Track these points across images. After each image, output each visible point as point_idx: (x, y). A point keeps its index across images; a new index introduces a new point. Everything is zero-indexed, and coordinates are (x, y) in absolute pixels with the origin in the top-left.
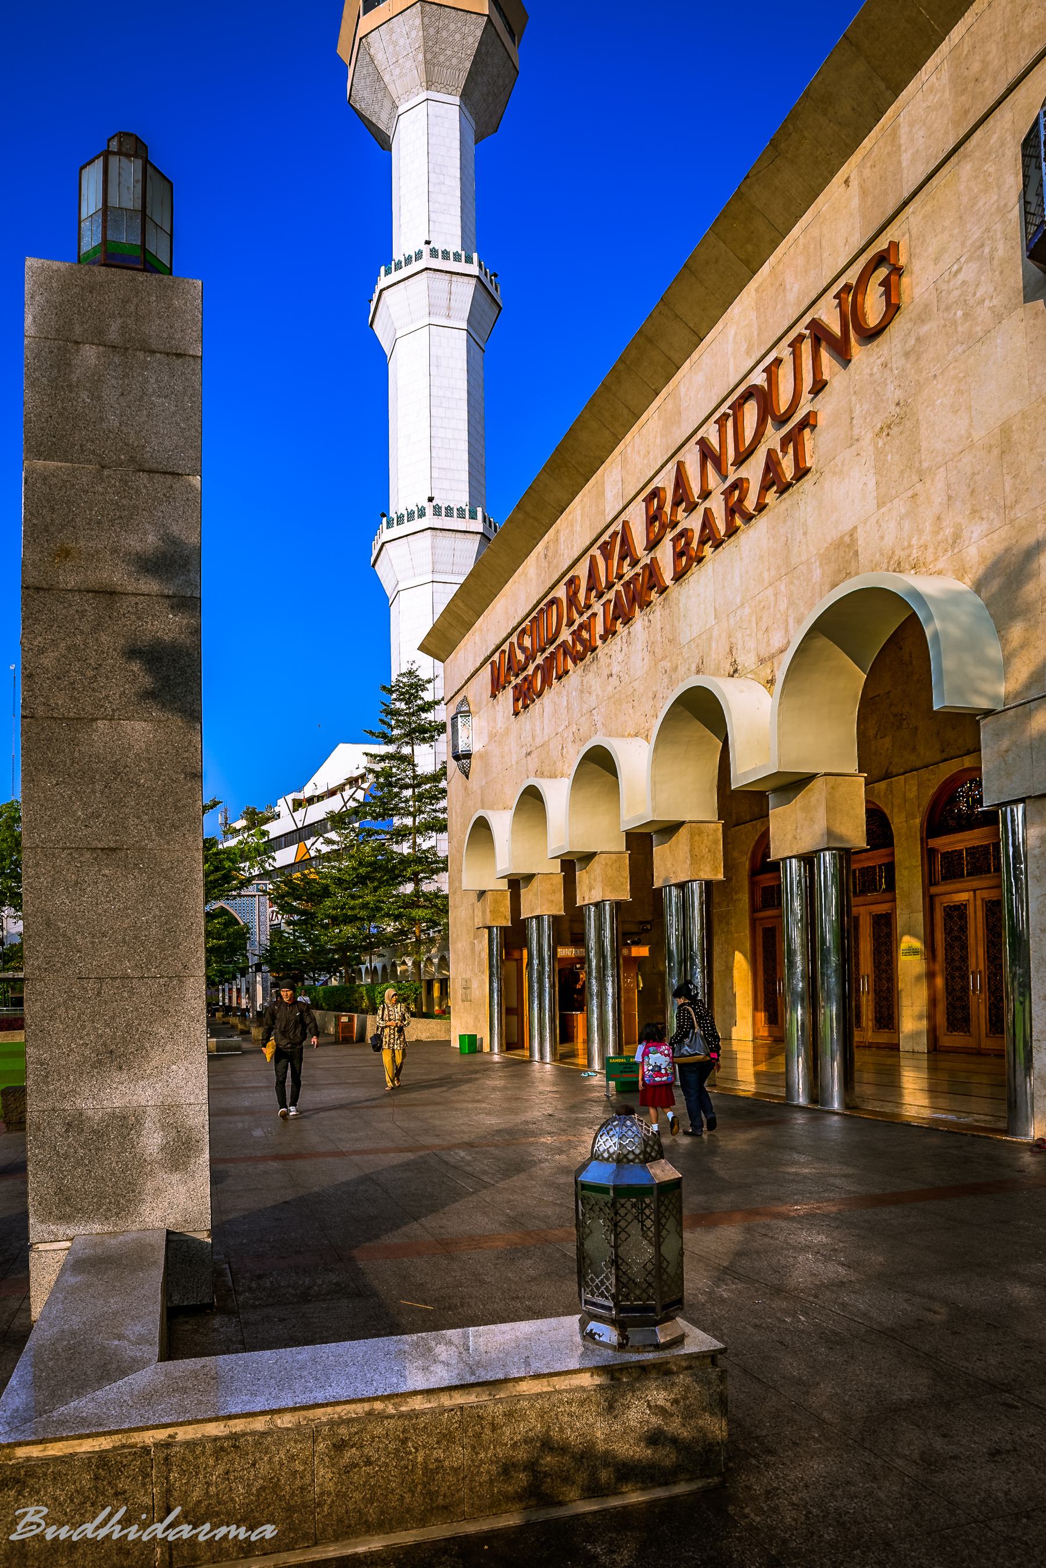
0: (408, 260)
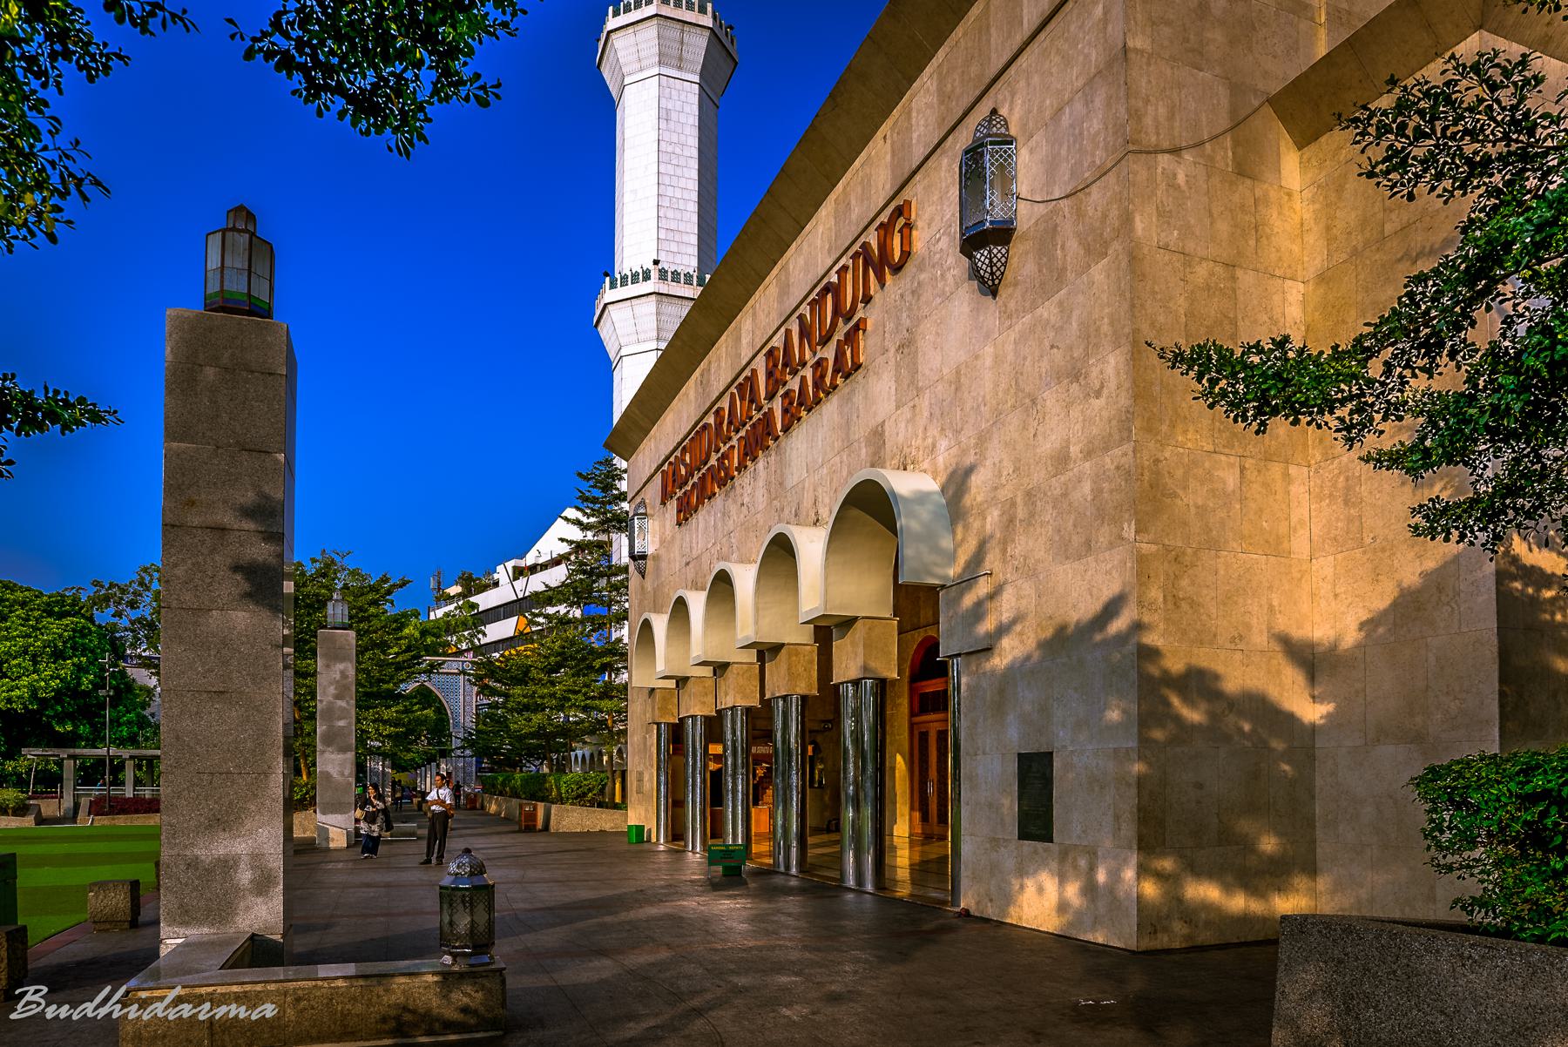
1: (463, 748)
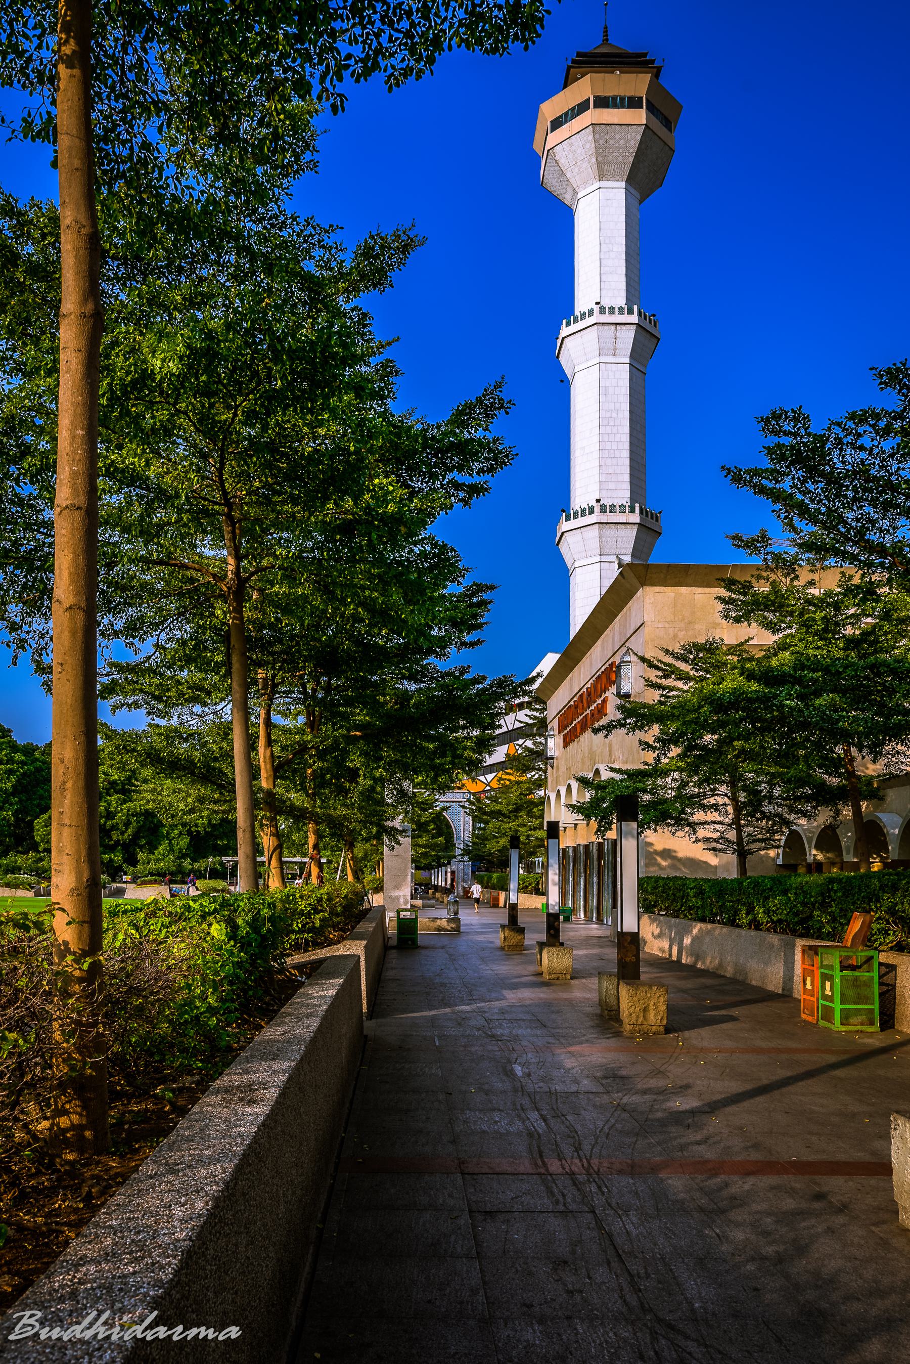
0: (583, 316)
1: (463, 855)
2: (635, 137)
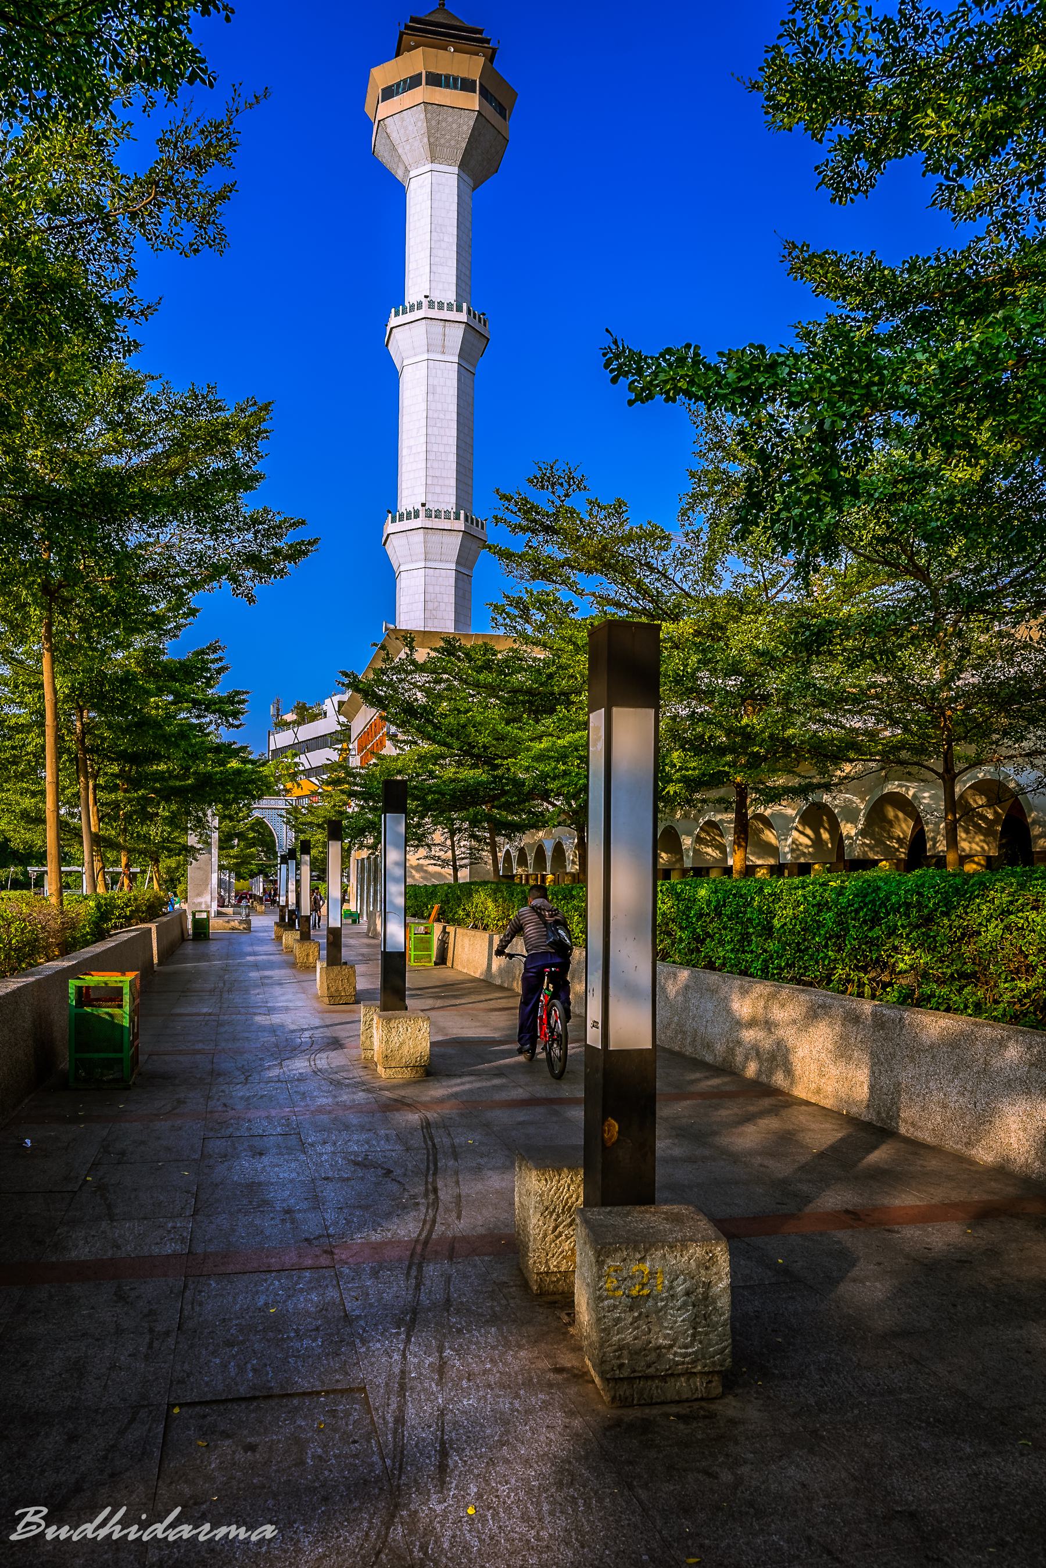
0: (412, 307)
2: (467, 123)
